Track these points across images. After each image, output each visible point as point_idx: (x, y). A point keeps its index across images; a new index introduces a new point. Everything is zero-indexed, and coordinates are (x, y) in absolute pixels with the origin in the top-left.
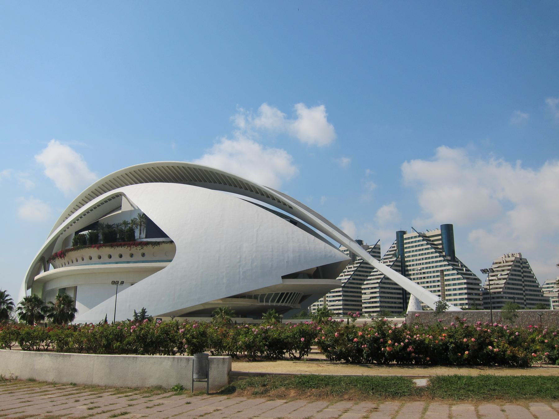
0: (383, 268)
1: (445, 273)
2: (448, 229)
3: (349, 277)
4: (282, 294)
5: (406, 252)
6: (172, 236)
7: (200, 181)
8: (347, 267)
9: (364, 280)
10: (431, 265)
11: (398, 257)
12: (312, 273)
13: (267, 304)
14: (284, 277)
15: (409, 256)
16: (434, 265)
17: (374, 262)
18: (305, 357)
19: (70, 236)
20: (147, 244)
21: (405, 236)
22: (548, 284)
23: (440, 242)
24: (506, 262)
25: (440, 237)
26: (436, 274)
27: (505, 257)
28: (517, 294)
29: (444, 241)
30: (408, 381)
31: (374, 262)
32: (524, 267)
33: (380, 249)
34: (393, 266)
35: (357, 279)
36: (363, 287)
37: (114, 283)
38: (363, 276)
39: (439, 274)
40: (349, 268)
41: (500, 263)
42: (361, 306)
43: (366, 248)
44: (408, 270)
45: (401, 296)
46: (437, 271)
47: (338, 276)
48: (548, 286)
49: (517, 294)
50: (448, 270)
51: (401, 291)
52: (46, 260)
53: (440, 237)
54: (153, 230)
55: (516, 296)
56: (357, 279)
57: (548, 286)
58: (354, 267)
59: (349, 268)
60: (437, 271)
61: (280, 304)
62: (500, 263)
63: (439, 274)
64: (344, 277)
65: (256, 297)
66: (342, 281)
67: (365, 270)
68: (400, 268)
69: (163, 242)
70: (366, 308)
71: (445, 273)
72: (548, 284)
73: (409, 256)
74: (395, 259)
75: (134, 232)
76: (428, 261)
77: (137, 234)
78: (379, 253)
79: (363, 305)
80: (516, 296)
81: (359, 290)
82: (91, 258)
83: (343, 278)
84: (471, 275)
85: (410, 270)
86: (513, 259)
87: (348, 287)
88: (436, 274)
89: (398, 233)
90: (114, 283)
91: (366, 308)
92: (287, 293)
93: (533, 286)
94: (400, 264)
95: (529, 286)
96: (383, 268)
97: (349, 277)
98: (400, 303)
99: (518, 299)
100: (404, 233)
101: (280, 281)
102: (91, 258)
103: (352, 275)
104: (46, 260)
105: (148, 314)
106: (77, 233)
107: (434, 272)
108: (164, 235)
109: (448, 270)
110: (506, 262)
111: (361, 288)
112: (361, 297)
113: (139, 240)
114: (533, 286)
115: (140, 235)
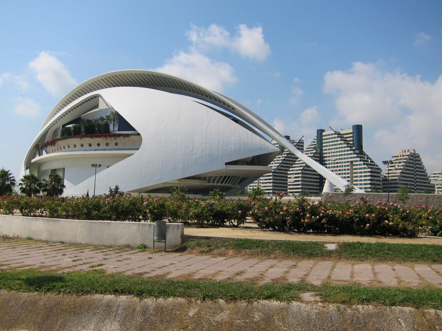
2: (358, 129)
13: (213, 184)
14: (227, 164)
18: (242, 225)
19: (59, 128)
20: (119, 135)
23: (352, 139)
24: (403, 156)
25: (352, 135)
28: (410, 181)
30: (320, 245)
32: (416, 160)
33: (303, 143)
37: (93, 165)
39: (349, 164)
41: (398, 157)
45: (318, 180)
46: (348, 162)
49: (410, 181)
51: (318, 177)
52: (40, 147)
53: (352, 135)
60: (348, 162)
62: (398, 157)
63: (349, 164)
65: (204, 179)
68: (319, 159)
69: (132, 134)
71: (354, 163)
75: (109, 126)
77: (111, 128)
78: (303, 146)
84: (374, 165)
89: (318, 131)
90: (93, 165)
94: (319, 155)
95: (419, 175)
99: (410, 185)
101: (224, 167)
104: (40, 147)
105: (4, 169)
106: (64, 126)
110: (403, 156)
113: (113, 133)
115: (113, 128)
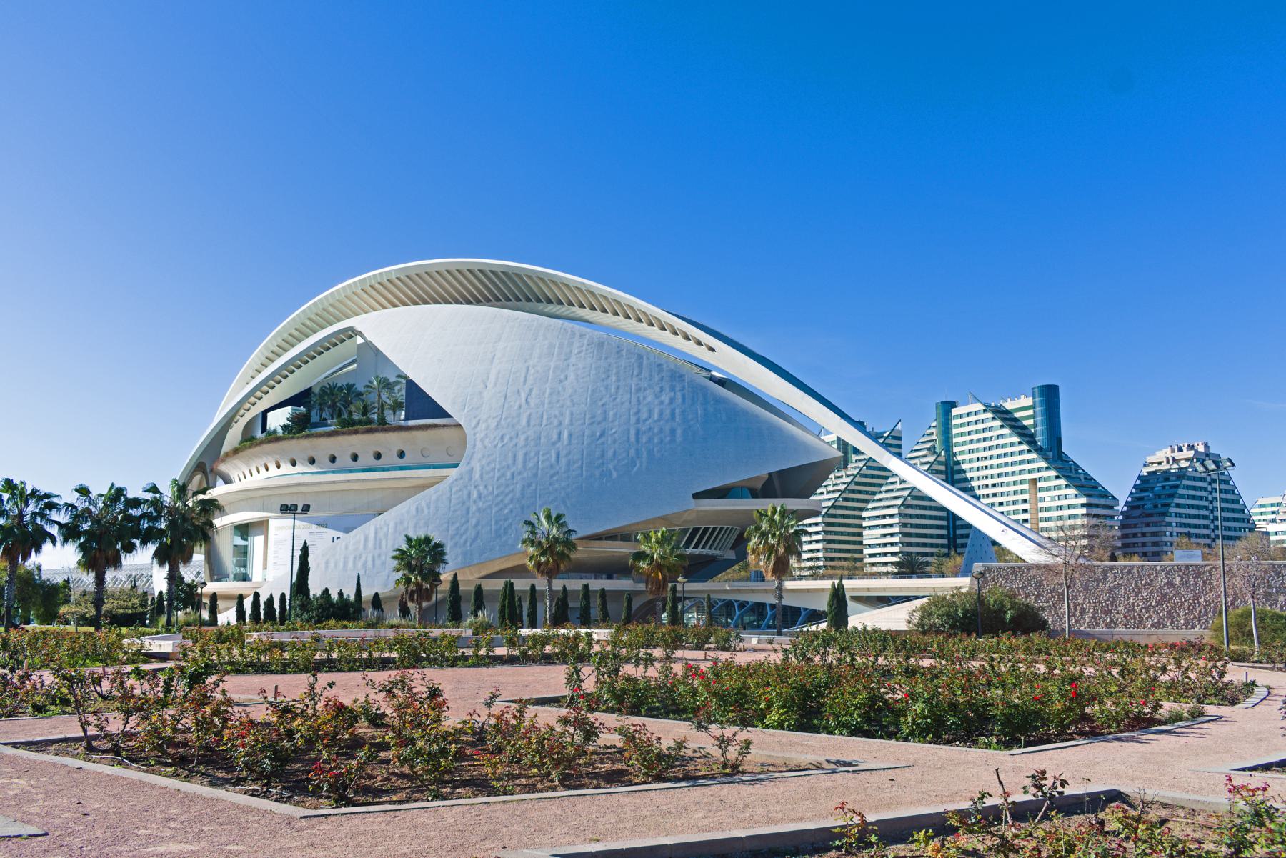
0: (912, 475)
1: (1039, 485)
3: (837, 495)
4: (695, 531)
5: (957, 444)
6: (458, 416)
7: (508, 300)
8: (832, 476)
9: (867, 501)
10: (981, 436)
11: (939, 455)
12: (759, 485)
14: (697, 496)
15: (961, 453)
16: (1017, 468)
17: (893, 464)
21: (955, 412)
22: (1262, 506)
26: (1019, 487)
27: (1173, 451)
28: (1196, 526)
29: (1039, 419)
31: (893, 464)
33: (899, 438)
34: (932, 471)
35: (853, 500)
36: (865, 514)
38: (867, 493)
39: (1026, 486)
40: (837, 477)
42: (861, 551)
43: (875, 437)
44: (958, 463)
46: (1022, 482)
47: (813, 493)
48: (1263, 510)
49: (1196, 526)
50: (1045, 479)
51: (944, 514)
54: (421, 405)
55: (1193, 531)
56: (853, 500)
57: (1263, 510)
58: (848, 476)
59: (837, 477)
60: (1022, 482)
61: (689, 551)
62: (1160, 463)
63: (1026, 486)
64: (825, 496)
66: (824, 504)
67: (876, 476)
69: (444, 426)
70: (871, 555)
71: (1039, 485)
72: (1262, 506)
73: (961, 453)
74: (931, 459)
76: (1003, 460)
78: (900, 446)
79: (866, 551)
80: (1193, 531)
81: (857, 522)
82: (333, 459)
83: (826, 495)
85: (964, 461)
86: (1191, 454)
87: (834, 516)
88: (1019, 487)
91: (871, 555)
92: (706, 529)
93: (1233, 510)
96: (912, 475)
97: (837, 495)
98: (943, 546)
100: (954, 405)
102: (333, 459)
103: (843, 492)
107: (1015, 483)
108: (445, 414)
109: (1045, 479)
111: (861, 518)
112: (860, 535)
114: (1233, 510)
